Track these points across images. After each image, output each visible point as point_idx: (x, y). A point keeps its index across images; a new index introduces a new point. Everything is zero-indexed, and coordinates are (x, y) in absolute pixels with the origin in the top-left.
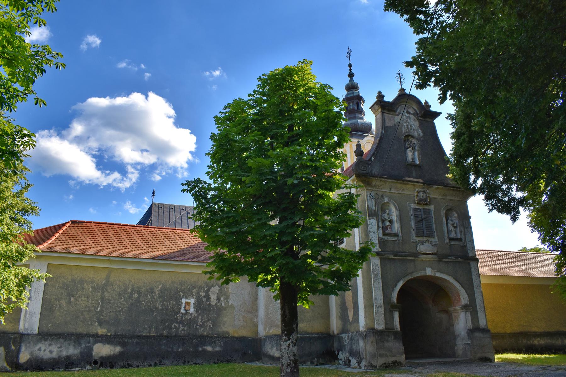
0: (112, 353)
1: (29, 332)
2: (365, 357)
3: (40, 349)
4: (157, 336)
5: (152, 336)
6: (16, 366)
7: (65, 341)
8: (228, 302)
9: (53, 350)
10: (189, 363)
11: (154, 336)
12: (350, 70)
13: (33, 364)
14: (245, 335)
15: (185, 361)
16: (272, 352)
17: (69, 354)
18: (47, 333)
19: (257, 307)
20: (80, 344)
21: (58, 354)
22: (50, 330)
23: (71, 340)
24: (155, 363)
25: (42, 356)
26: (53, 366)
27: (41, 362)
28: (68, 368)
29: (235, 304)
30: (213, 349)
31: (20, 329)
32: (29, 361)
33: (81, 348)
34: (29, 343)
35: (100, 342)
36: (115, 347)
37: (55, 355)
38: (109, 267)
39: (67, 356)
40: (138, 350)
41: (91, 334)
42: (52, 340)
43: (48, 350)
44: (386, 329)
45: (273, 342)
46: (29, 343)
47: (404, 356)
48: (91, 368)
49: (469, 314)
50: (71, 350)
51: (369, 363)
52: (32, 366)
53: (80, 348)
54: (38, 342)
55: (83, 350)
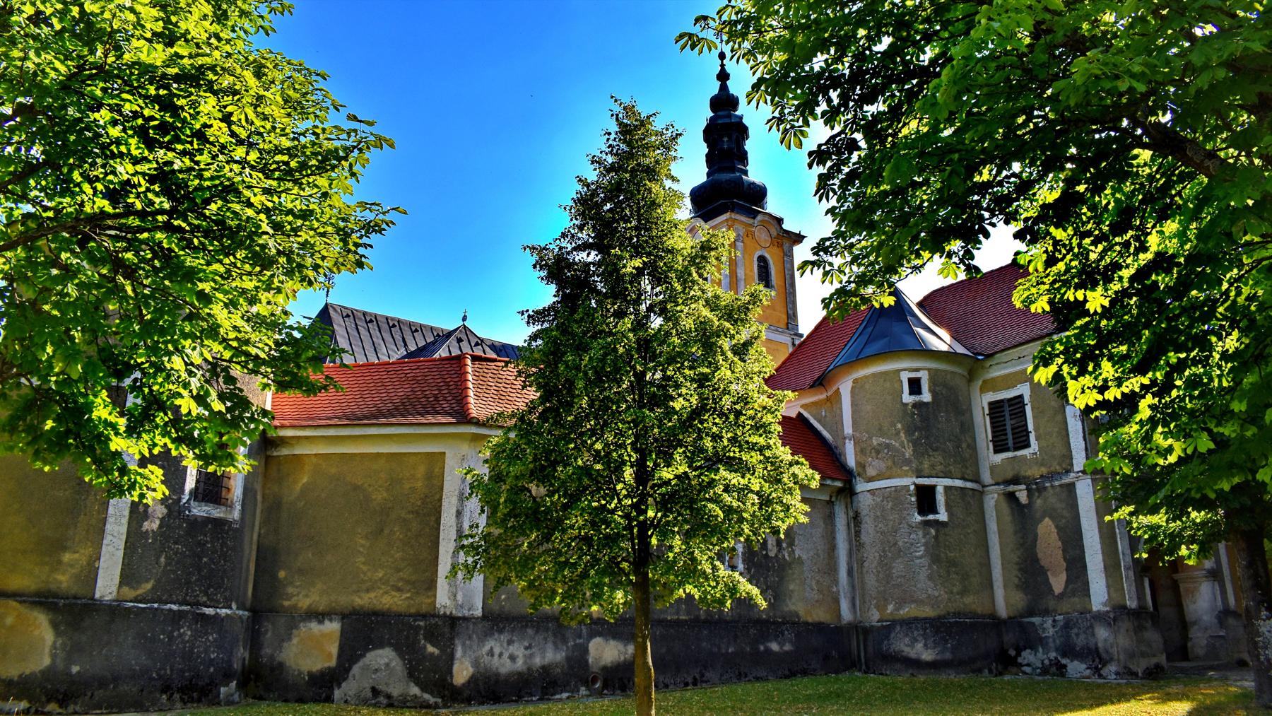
0: (622, 658)
1: (466, 613)
2: (1116, 657)
3: (491, 653)
4: (690, 620)
6: (454, 696)
7: (537, 632)
9: (516, 653)
10: (746, 676)
11: (686, 621)
12: (722, 66)
13: (482, 687)
14: (822, 620)
15: (740, 674)
16: (914, 651)
18: (499, 615)
19: (835, 562)
20: (565, 641)
21: (525, 662)
22: (503, 607)
23: (547, 629)
24: (695, 678)
27: (497, 682)
28: (547, 694)
29: (804, 557)
30: (781, 648)
31: (438, 606)
32: (473, 680)
33: (567, 647)
34: (470, 638)
35: (600, 634)
37: (520, 664)
39: (543, 667)
42: (513, 631)
43: (506, 655)
46: (470, 638)
48: (588, 693)
51: (1125, 667)
52: (479, 692)
53: (565, 648)
54: (486, 636)
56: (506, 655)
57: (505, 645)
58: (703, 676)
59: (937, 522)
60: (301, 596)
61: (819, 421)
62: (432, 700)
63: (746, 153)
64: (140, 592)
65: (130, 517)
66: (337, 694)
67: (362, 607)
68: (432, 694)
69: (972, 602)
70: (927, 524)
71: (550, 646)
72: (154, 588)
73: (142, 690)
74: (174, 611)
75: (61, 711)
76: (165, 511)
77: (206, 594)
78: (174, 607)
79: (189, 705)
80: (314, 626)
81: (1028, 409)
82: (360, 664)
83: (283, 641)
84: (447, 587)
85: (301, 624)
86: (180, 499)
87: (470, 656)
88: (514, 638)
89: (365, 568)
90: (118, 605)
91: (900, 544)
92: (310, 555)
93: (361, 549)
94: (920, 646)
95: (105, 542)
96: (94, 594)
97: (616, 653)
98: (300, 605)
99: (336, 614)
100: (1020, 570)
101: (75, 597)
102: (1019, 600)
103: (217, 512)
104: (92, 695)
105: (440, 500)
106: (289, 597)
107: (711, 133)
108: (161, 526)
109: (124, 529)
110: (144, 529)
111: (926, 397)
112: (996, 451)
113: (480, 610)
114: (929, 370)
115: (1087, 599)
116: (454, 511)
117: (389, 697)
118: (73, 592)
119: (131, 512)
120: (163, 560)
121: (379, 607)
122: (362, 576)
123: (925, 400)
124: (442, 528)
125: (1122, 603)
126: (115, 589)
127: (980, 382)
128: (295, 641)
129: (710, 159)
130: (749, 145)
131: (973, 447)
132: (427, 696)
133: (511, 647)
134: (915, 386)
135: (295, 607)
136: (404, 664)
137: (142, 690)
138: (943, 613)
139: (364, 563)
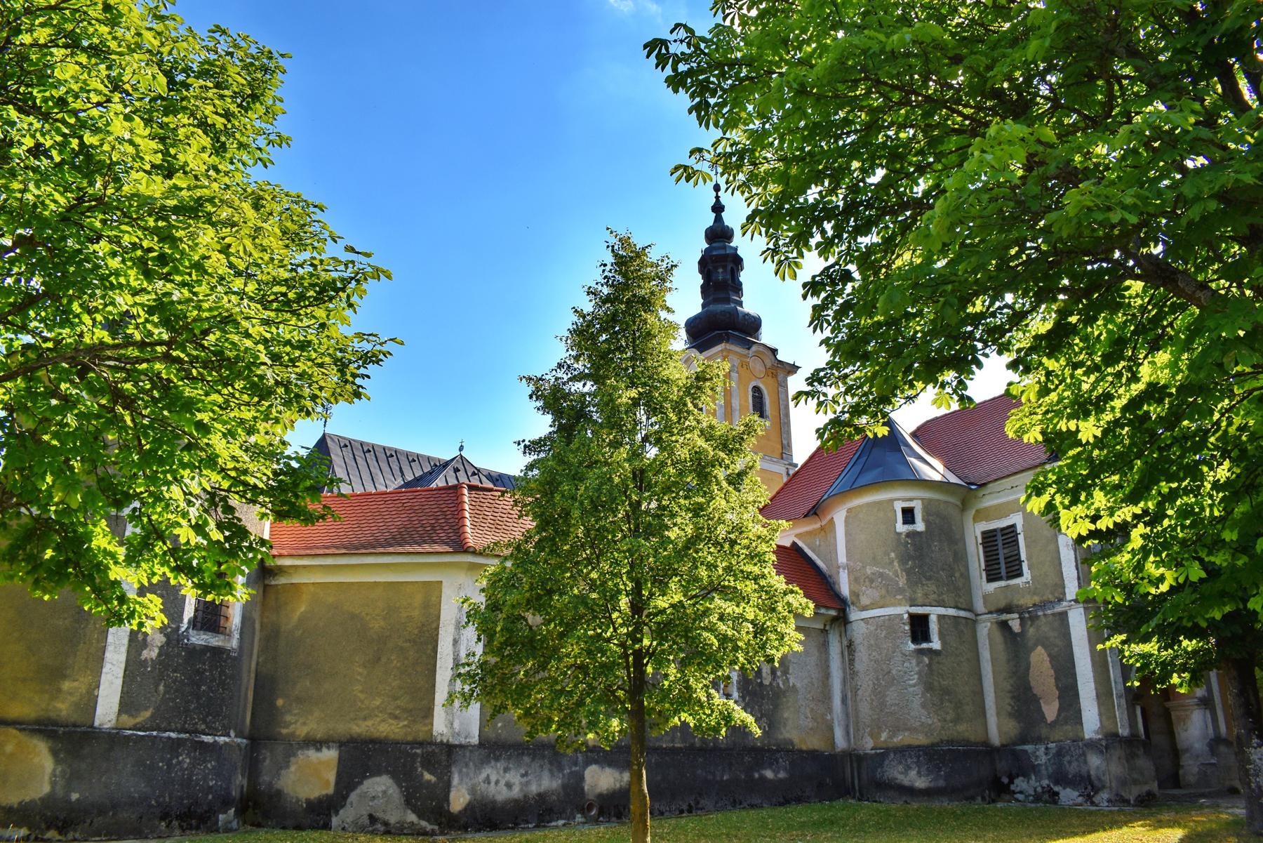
0: (618, 785)
1: (463, 741)
2: (1108, 785)
3: (487, 781)
5: (678, 748)
7: (533, 760)
8: (788, 679)
9: (512, 781)
12: (717, 197)
14: (816, 748)
16: (908, 778)
18: (495, 743)
20: (561, 769)
21: (521, 790)
23: (543, 757)
24: (690, 805)
26: (516, 818)
29: (798, 685)
31: (435, 733)
32: (469, 808)
33: (564, 775)
34: (467, 765)
35: (596, 762)
36: (621, 773)
37: (516, 792)
39: (540, 795)
40: (659, 778)
42: (509, 758)
43: (502, 782)
45: (909, 760)
46: (467, 765)
47: (1156, 784)
48: (583, 820)
49: (1208, 712)
50: (546, 782)
51: (1117, 795)
53: (561, 775)
54: (482, 764)
55: (566, 781)
56: (502, 782)
57: (501, 772)
59: (930, 650)
61: (813, 551)
62: (429, 827)
63: (740, 284)
64: (139, 720)
65: (130, 645)
66: (335, 821)
67: (359, 735)
68: (428, 821)
69: (965, 730)
70: (921, 652)
72: (153, 716)
73: (141, 818)
75: (60, 838)
76: (164, 639)
77: (204, 722)
80: (312, 754)
81: (1021, 538)
82: (358, 791)
83: (281, 768)
85: (299, 752)
86: (178, 628)
87: (467, 784)
88: (511, 766)
89: (362, 696)
90: (117, 733)
91: (894, 672)
94: (913, 773)
95: (104, 670)
97: (612, 780)
99: (333, 742)
100: (1013, 697)
101: (75, 725)
102: (1012, 727)
103: (215, 641)
107: (706, 265)
108: (160, 655)
109: (123, 657)
110: (143, 658)
111: (920, 526)
112: (990, 580)
113: (477, 738)
114: (922, 499)
115: (1079, 727)
117: (386, 824)
119: (130, 641)
120: (161, 688)
121: (376, 735)
123: (919, 530)
124: (438, 656)
125: (1114, 731)
126: (113, 717)
127: (974, 512)
128: (293, 768)
129: (705, 290)
130: (744, 277)
131: (966, 577)
132: (424, 823)
134: (908, 515)
135: (293, 734)
136: (401, 791)
137: (141, 818)
138: (936, 741)
139: (361, 692)
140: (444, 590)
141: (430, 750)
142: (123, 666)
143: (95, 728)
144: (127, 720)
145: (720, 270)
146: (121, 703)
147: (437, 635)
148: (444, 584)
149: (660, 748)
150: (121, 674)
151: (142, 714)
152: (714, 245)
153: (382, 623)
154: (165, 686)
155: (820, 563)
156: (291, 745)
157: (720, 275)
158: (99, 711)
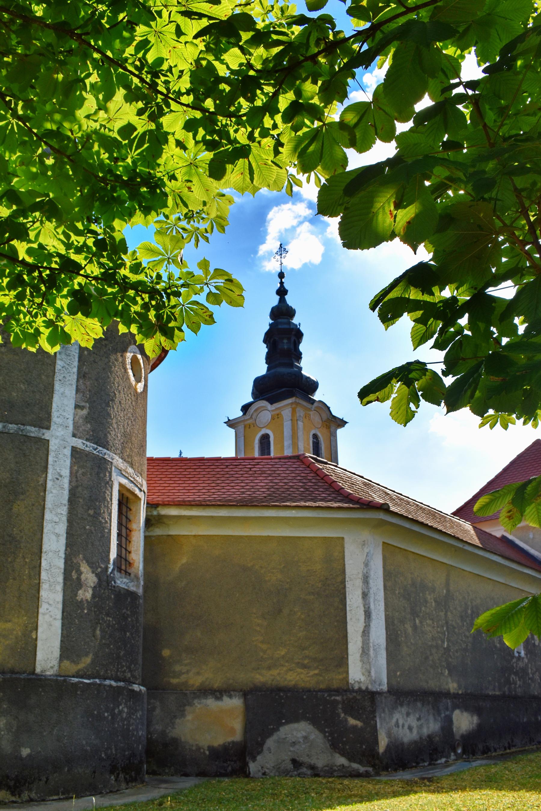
3: (397, 725)
12: (282, 283)
17: (430, 733)
20: (439, 714)
25: (402, 738)
31: (350, 681)
34: (384, 711)
36: (472, 716)
38: (448, 563)
41: (356, 687)
44: (74, 115)
53: (439, 718)
57: (405, 717)
58: (512, 741)
60: (191, 674)
61: (526, 542)
62: (362, 769)
63: (301, 354)
64: (81, 666)
65: (65, 584)
66: (253, 767)
68: (361, 763)
71: (431, 718)
72: (93, 662)
73: (94, 772)
74: (114, 687)
75: (13, 799)
76: (95, 580)
78: (113, 683)
79: (130, 784)
80: (211, 702)
82: (275, 737)
83: (175, 717)
84: (359, 664)
85: (196, 701)
86: (107, 568)
88: (410, 711)
89: (264, 647)
90: (65, 681)
92: (199, 634)
93: (258, 629)
95: (41, 610)
96: (35, 670)
98: (191, 682)
99: (234, 690)
101: (12, 672)
104: (47, 779)
105: (343, 582)
106: (178, 675)
108: (94, 596)
109: (59, 597)
110: (79, 598)
113: (386, 685)
116: (359, 593)
117: (312, 767)
118: (10, 666)
119: (65, 579)
120: (98, 632)
121: (283, 684)
122: (261, 654)
124: (348, 608)
128: (189, 717)
129: (269, 359)
132: (355, 766)
133: (409, 719)
135: (185, 684)
136: (325, 736)
137: (94, 772)
139: (262, 642)
140: (347, 546)
141: (351, 697)
142: (60, 606)
143: (37, 675)
144: (70, 667)
145: (285, 341)
146: (62, 648)
147: (345, 587)
148: (346, 540)
149: (488, 696)
150: (59, 615)
151: (83, 660)
152: (280, 320)
153: (279, 576)
154: (102, 631)
155: (533, 551)
156: (186, 694)
157: (285, 344)
158: (40, 656)
